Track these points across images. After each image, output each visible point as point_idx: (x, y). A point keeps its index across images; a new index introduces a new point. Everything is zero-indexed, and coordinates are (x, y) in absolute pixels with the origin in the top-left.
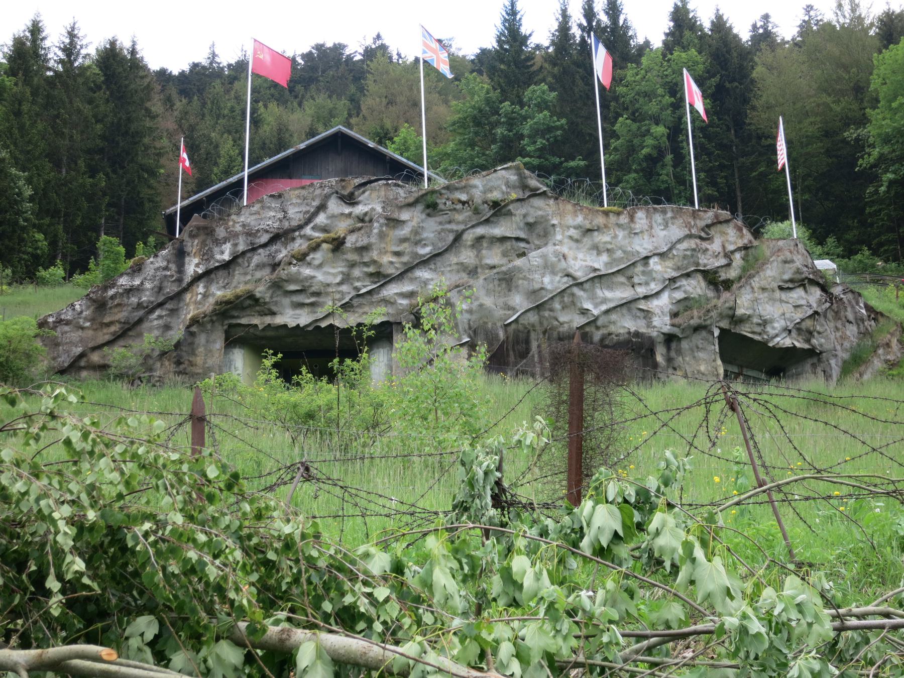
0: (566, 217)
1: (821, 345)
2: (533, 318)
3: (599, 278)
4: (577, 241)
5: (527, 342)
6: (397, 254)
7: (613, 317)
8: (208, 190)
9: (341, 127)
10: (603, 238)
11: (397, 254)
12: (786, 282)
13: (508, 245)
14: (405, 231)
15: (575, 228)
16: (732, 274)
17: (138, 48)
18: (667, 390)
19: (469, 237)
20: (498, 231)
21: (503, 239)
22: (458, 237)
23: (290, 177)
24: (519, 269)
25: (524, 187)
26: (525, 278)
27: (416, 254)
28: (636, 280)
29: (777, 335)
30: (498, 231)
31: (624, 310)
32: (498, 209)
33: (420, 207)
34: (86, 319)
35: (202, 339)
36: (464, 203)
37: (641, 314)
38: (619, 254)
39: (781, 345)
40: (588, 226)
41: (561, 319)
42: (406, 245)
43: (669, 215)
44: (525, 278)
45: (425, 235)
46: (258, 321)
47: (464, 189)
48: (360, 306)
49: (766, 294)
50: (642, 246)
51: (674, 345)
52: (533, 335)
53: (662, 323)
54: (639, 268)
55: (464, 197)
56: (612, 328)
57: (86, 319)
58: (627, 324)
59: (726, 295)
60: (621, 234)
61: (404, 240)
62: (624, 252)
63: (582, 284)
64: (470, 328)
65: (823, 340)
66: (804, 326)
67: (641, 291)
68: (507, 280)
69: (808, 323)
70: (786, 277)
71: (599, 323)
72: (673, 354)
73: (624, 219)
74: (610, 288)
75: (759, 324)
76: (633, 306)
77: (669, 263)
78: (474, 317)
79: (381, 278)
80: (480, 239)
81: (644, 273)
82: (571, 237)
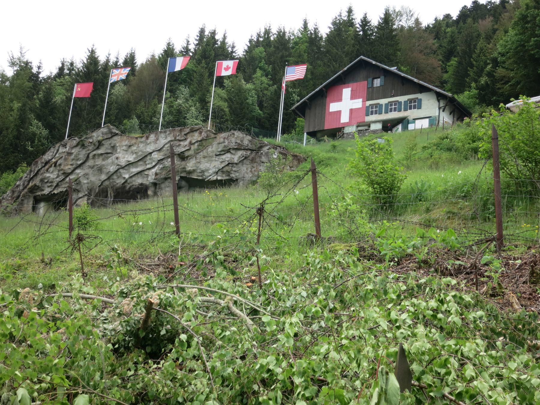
0: (121, 142)
1: (236, 176)
2: (107, 183)
3: (130, 164)
4: (126, 151)
5: (107, 192)
6: (72, 165)
7: (134, 179)
8: (410, 77)
9: (362, 57)
10: (134, 148)
11: (72, 165)
12: (221, 151)
13: (103, 156)
14: (72, 157)
15: (125, 146)
16: (191, 152)
17: (367, 16)
18: (467, 170)
19: (91, 155)
20: (100, 152)
21: (102, 154)
22: (88, 157)
23: (345, 84)
24: (104, 165)
25: (111, 133)
26: (105, 168)
27: (77, 164)
28: (147, 163)
29: (210, 176)
30: (100, 152)
31: (139, 175)
32: (100, 144)
33: (79, 146)
34: (9, 197)
35: (26, 201)
36: (91, 143)
37: (145, 176)
38: (140, 153)
39: (211, 179)
40: (129, 145)
41: (117, 182)
42: (74, 161)
43: (168, 133)
44: (105, 168)
45: (80, 156)
46: (39, 193)
47: (91, 137)
48: (61, 185)
49: (206, 159)
50: (149, 149)
51: (158, 187)
52: (109, 189)
53: (151, 179)
54: (149, 157)
55: (91, 141)
56: (134, 183)
57: (9, 197)
58: (139, 181)
59: (183, 163)
60: (141, 145)
61: (73, 160)
62: (143, 152)
63: (124, 167)
64: (88, 189)
65: (238, 174)
66: (225, 169)
67: (149, 166)
68: (100, 170)
69: (227, 168)
70: (219, 150)
71: (128, 182)
72: (157, 190)
73: (143, 139)
74: (136, 167)
75: (200, 172)
76: (142, 173)
77: (162, 153)
78: (89, 185)
79: (67, 175)
80: (95, 155)
81: (150, 159)
82: (123, 150)
